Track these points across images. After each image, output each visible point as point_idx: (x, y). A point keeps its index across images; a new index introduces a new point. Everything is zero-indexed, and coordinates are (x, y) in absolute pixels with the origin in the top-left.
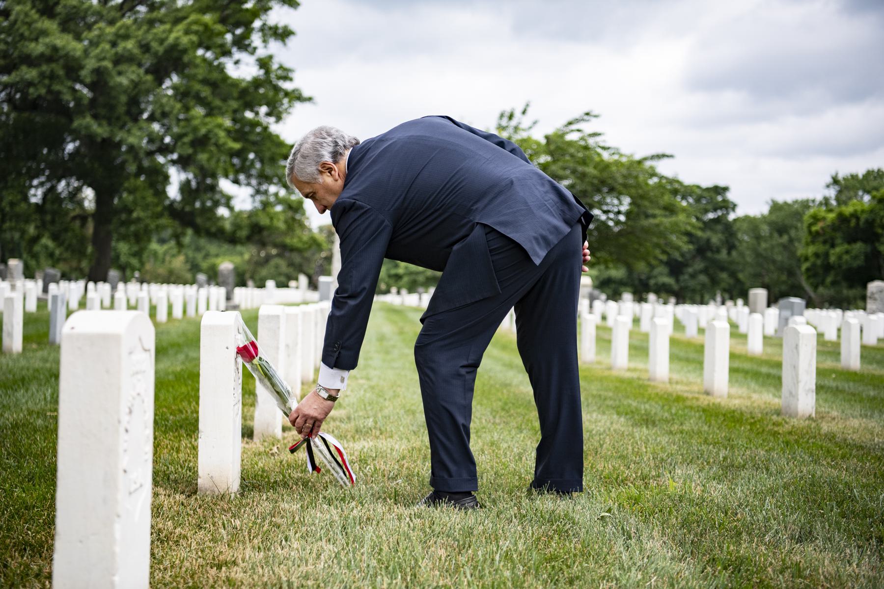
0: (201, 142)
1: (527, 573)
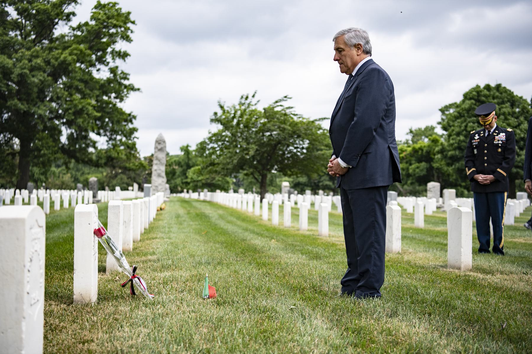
0: (79, 113)
1: (251, 339)
